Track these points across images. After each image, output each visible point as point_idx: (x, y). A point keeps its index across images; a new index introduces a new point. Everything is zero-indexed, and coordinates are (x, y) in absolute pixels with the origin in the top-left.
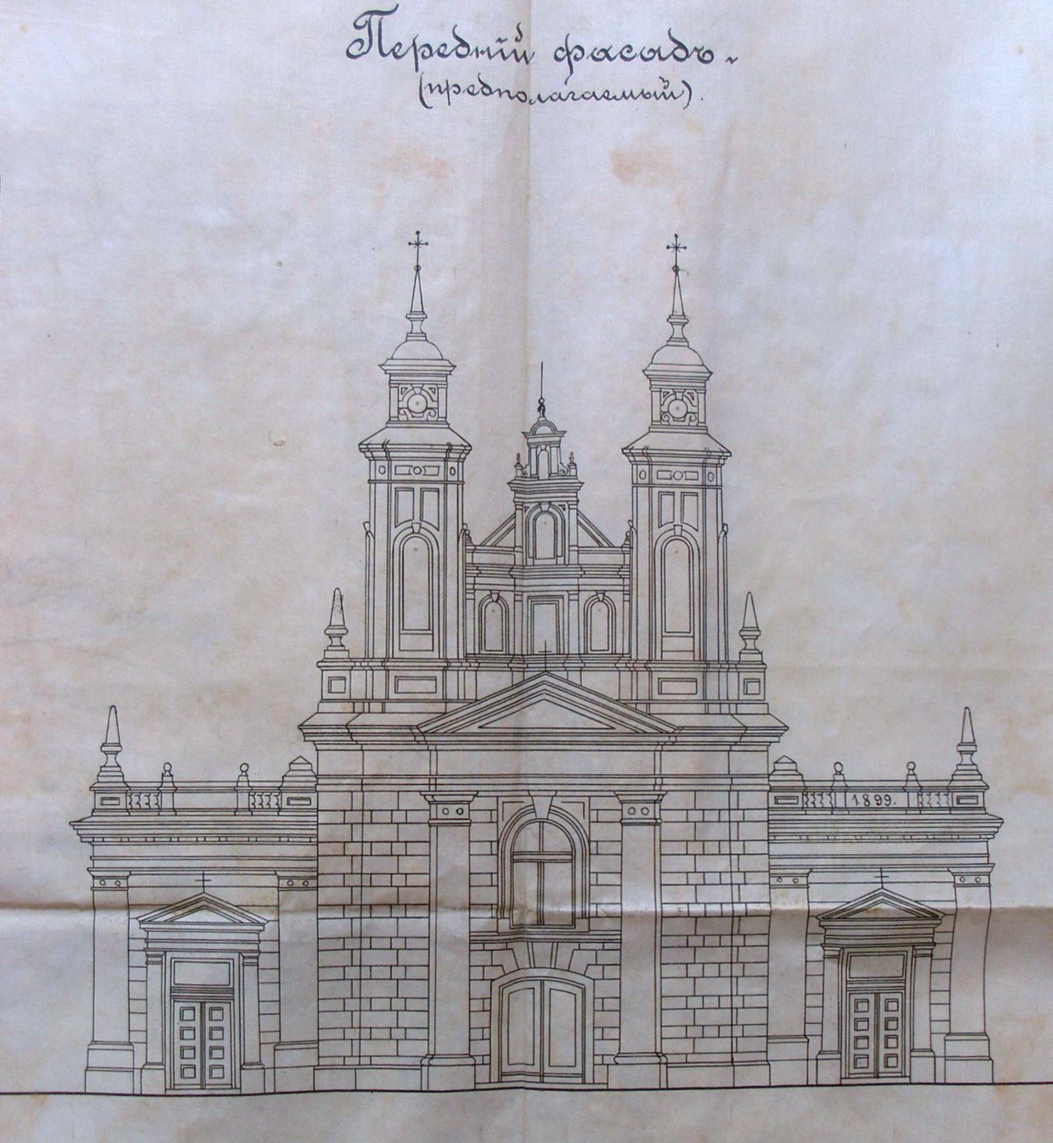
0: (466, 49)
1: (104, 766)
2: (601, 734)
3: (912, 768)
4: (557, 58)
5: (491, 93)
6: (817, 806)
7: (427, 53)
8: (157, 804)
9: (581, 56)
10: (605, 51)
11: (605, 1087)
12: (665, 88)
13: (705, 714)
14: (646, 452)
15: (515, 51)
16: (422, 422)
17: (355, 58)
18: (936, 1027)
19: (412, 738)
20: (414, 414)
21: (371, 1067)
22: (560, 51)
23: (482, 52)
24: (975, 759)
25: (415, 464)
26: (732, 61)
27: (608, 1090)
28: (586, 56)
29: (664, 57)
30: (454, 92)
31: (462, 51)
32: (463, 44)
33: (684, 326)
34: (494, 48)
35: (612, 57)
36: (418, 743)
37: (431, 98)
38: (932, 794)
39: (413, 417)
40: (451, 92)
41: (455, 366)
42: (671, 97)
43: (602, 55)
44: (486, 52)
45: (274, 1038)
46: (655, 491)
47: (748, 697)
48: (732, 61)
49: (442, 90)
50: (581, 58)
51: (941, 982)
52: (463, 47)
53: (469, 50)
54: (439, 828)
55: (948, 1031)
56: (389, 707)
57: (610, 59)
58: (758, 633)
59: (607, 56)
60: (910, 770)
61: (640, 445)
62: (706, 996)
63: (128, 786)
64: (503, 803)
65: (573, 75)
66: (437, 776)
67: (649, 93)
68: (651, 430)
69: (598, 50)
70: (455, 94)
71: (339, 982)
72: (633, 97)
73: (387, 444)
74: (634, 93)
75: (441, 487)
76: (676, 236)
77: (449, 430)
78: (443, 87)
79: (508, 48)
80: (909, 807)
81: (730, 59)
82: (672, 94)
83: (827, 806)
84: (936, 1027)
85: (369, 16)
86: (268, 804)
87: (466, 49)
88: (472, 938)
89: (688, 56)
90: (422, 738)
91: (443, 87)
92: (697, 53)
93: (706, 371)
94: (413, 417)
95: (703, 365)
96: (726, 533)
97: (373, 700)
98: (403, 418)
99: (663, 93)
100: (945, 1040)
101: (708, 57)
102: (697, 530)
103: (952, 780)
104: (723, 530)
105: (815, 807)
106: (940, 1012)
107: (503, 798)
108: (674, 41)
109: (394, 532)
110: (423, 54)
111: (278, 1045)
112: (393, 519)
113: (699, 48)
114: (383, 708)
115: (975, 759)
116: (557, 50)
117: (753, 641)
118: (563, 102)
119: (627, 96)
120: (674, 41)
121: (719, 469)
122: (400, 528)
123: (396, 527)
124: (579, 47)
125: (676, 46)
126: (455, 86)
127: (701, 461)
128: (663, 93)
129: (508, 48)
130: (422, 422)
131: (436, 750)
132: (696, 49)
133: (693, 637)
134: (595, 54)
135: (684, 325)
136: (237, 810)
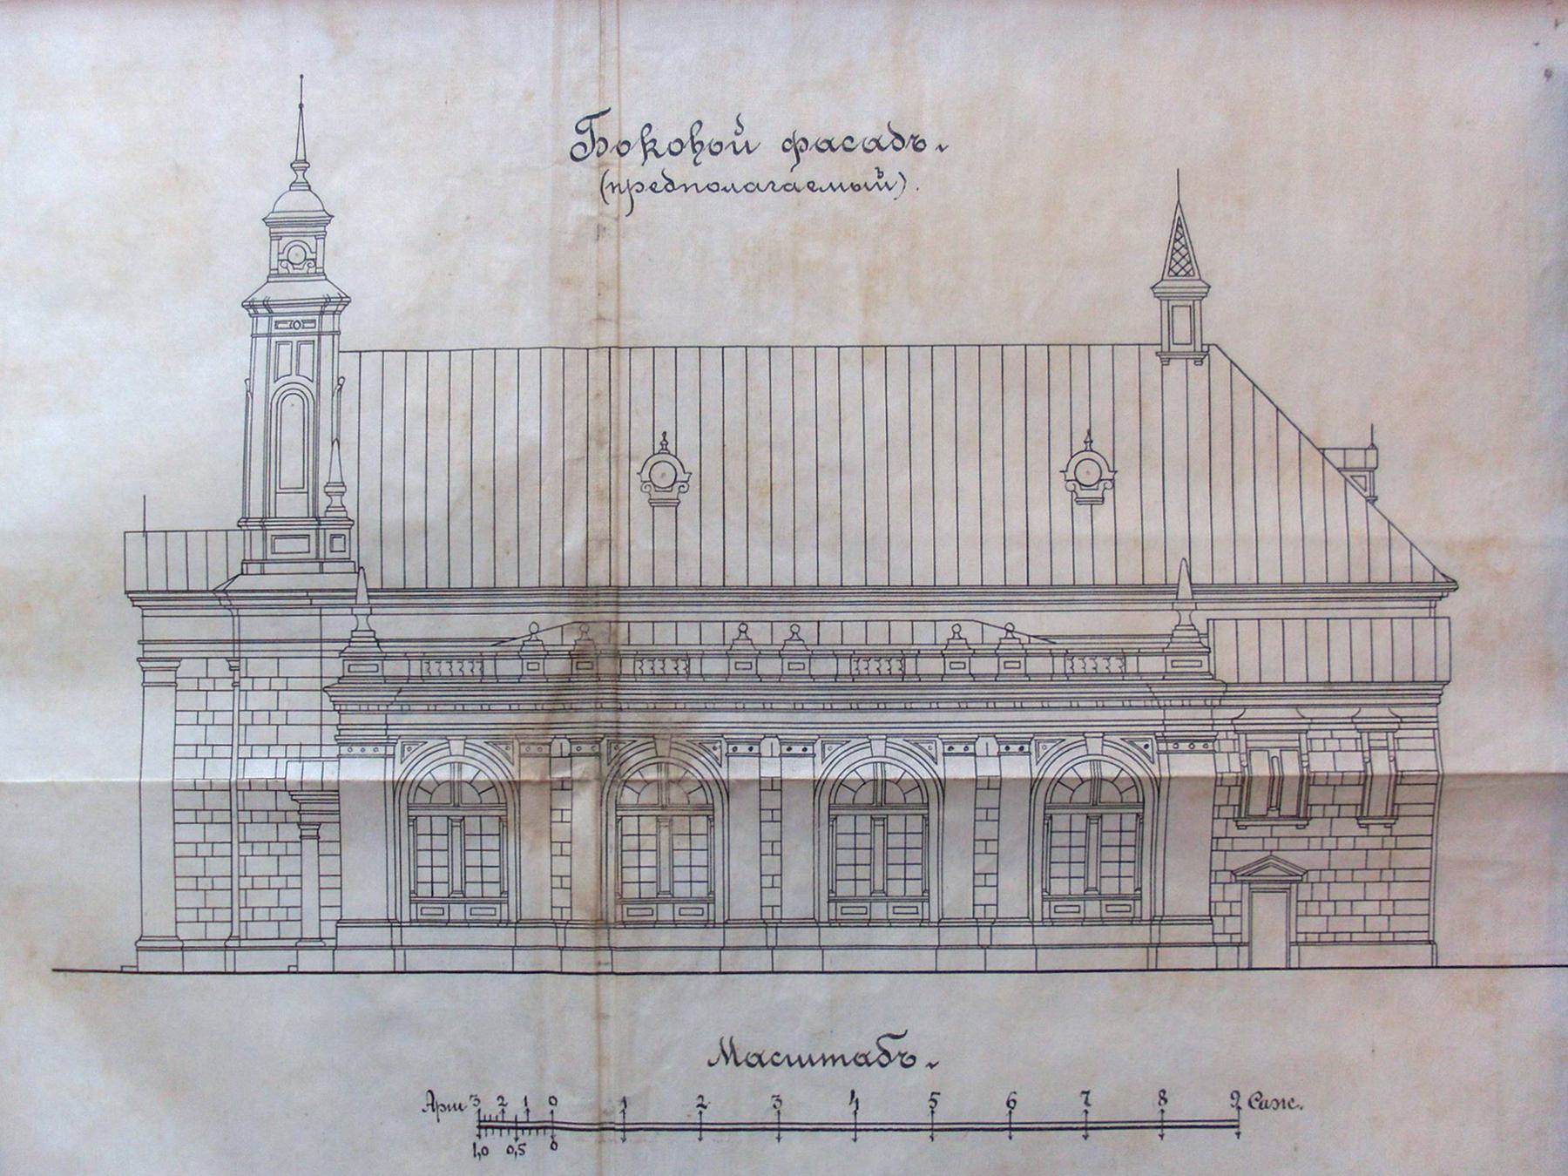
1: (356, 630)
2: (1275, 592)
5: (860, 189)
6: (680, 673)
7: (804, 148)
8: (900, 669)
10: (829, 143)
11: (135, 970)
12: (879, 177)
13: (261, 574)
14: (266, 304)
15: (734, 143)
16: (303, 275)
18: (326, 914)
19: (218, 603)
20: (295, 266)
21: (280, 943)
22: (787, 143)
25: (294, 318)
26: (942, 150)
27: (137, 973)
30: (637, 191)
33: (305, 171)
36: (225, 607)
38: (1112, 658)
39: (294, 269)
41: (332, 216)
45: (335, 914)
46: (274, 339)
47: (275, 557)
48: (942, 150)
51: (330, 865)
55: (339, 918)
56: (268, 568)
57: (833, 150)
58: (343, 489)
59: (878, 145)
61: (259, 297)
62: (750, 347)
66: (240, 641)
68: (270, 279)
71: (1209, 865)
73: (268, 301)
75: (316, 338)
76: (302, 76)
77: (326, 282)
78: (624, 186)
80: (1054, 673)
83: (446, 674)
84: (326, 914)
85: (589, 121)
86: (857, 669)
88: (335, 807)
90: (228, 603)
91: (624, 186)
93: (326, 215)
94: (294, 269)
95: (324, 210)
96: (340, 389)
97: (251, 561)
98: (282, 271)
99: (877, 183)
100: (337, 927)
101: (921, 146)
102: (312, 381)
103: (524, 645)
104: (339, 384)
105: (880, 675)
106: (330, 897)
109: (273, 387)
111: (340, 923)
112: (273, 374)
114: (262, 568)
116: (575, 146)
121: (336, 316)
122: (279, 383)
123: (275, 382)
127: (319, 309)
128: (877, 183)
130: (303, 275)
131: (239, 616)
133: (308, 493)
135: (305, 170)
136: (837, 676)
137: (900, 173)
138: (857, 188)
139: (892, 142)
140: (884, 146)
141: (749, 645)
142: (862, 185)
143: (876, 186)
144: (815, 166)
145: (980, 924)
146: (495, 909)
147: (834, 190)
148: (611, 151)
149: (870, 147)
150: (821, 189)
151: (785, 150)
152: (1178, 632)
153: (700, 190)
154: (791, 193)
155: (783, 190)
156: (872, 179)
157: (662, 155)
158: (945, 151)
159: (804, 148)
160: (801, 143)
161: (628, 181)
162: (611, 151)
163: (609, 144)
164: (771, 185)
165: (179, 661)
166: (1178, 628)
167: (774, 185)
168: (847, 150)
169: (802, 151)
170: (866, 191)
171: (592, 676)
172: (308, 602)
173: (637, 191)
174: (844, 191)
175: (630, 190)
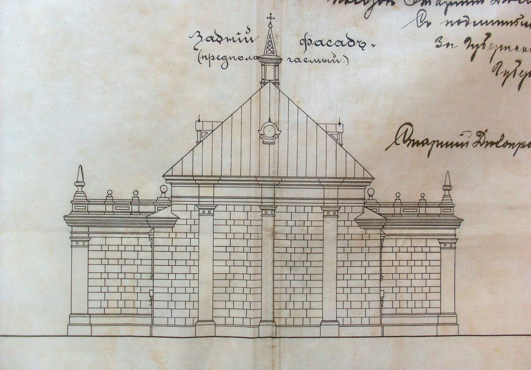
0: (353, 43)
3: (423, 196)
4: (301, 44)
7: (310, 43)
9: (310, 44)
10: (321, 41)
15: (246, 38)
17: (317, 46)
22: (302, 41)
23: (230, 40)
24: (84, 189)
26: (374, 46)
28: (312, 43)
29: (344, 45)
31: (351, 44)
32: (352, 40)
34: (236, 38)
35: (324, 45)
37: (203, 61)
40: (211, 59)
42: (318, 62)
43: (319, 43)
44: (232, 40)
48: (374, 46)
49: (207, 58)
50: (310, 45)
52: (351, 42)
53: (354, 43)
54: (105, 211)
57: (323, 45)
60: (422, 197)
63: (386, 219)
64: (129, 207)
65: (306, 51)
67: (325, 60)
69: (318, 41)
70: (212, 60)
72: (319, 62)
74: (250, 57)
79: (242, 37)
81: (373, 45)
82: (337, 60)
87: (353, 43)
89: (354, 45)
91: (207, 57)
92: (359, 43)
99: (333, 60)
107: (131, 207)
108: (348, 38)
110: (308, 43)
113: (359, 41)
115: (84, 189)
117: (78, 181)
118: (311, 63)
119: (316, 61)
120: (348, 38)
124: (310, 40)
125: (349, 40)
126: (213, 56)
128: (333, 60)
129: (242, 37)
132: (358, 41)
134: (316, 43)
137: (343, 56)
138: (325, 61)
139: (348, 43)
140: (324, 45)
141: (90, 201)
142: (327, 60)
143: (333, 61)
144: (315, 52)
145: (425, 203)
146: (417, 209)
147: (320, 62)
148: (313, 45)
149: (318, 44)
150: (310, 61)
151: (301, 44)
152: (77, 194)
153: (330, 62)
154: (298, 63)
155: (222, 59)
156: (331, 58)
157: (236, 41)
158: (242, 42)
159: (310, 43)
160: (309, 41)
161: (209, 54)
162: (313, 45)
163: (312, 42)
164: (289, 59)
165: (365, 187)
166: (77, 193)
167: (290, 59)
168: (328, 45)
169: (308, 45)
170: (250, 60)
171: (86, 212)
172: (320, 180)
173: (212, 59)
174: (235, 60)
175: (210, 58)
